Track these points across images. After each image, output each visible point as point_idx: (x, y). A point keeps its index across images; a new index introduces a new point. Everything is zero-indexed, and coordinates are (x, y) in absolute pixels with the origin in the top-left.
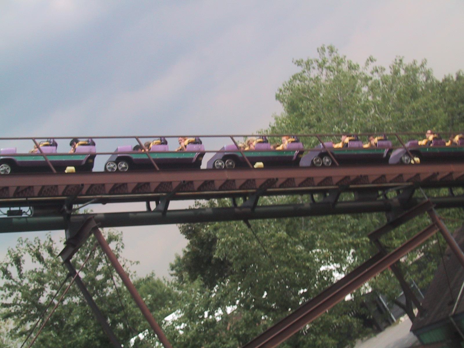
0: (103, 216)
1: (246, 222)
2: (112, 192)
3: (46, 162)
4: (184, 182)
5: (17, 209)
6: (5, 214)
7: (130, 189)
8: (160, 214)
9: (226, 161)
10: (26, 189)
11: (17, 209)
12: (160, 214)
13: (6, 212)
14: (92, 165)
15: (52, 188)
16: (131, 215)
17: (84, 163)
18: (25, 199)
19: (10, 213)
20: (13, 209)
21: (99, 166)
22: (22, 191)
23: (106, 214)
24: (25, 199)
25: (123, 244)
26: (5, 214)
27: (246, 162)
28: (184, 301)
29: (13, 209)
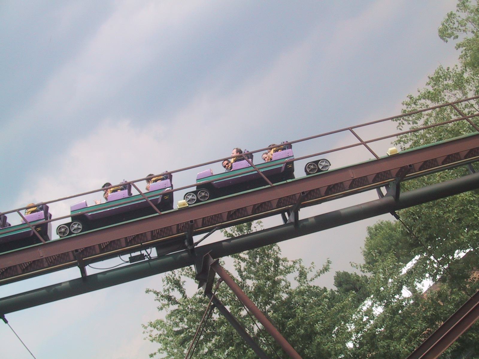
0: (313, 220)
1: (393, 214)
2: (351, 187)
3: (258, 174)
4: (303, 193)
5: (138, 253)
6: (127, 262)
7: (371, 180)
8: (292, 226)
9: (67, 226)
10: (30, 265)
11: (138, 253)
12: (292, 226)
13: (128, 260)
14: (292, 170)
15: (212, 219)
16: (99, 276)
17: (283, 170)
18: (140, 244)
19: (132, 259)
20: (133, 254)
21: (179, 202)
22: (258, 208)
23: (316, 217)
24: (140, 244)
25: (278, 247)
26: (127, 262)
27: (262, 178)
28: (296, 274)
29: (133, 254)
